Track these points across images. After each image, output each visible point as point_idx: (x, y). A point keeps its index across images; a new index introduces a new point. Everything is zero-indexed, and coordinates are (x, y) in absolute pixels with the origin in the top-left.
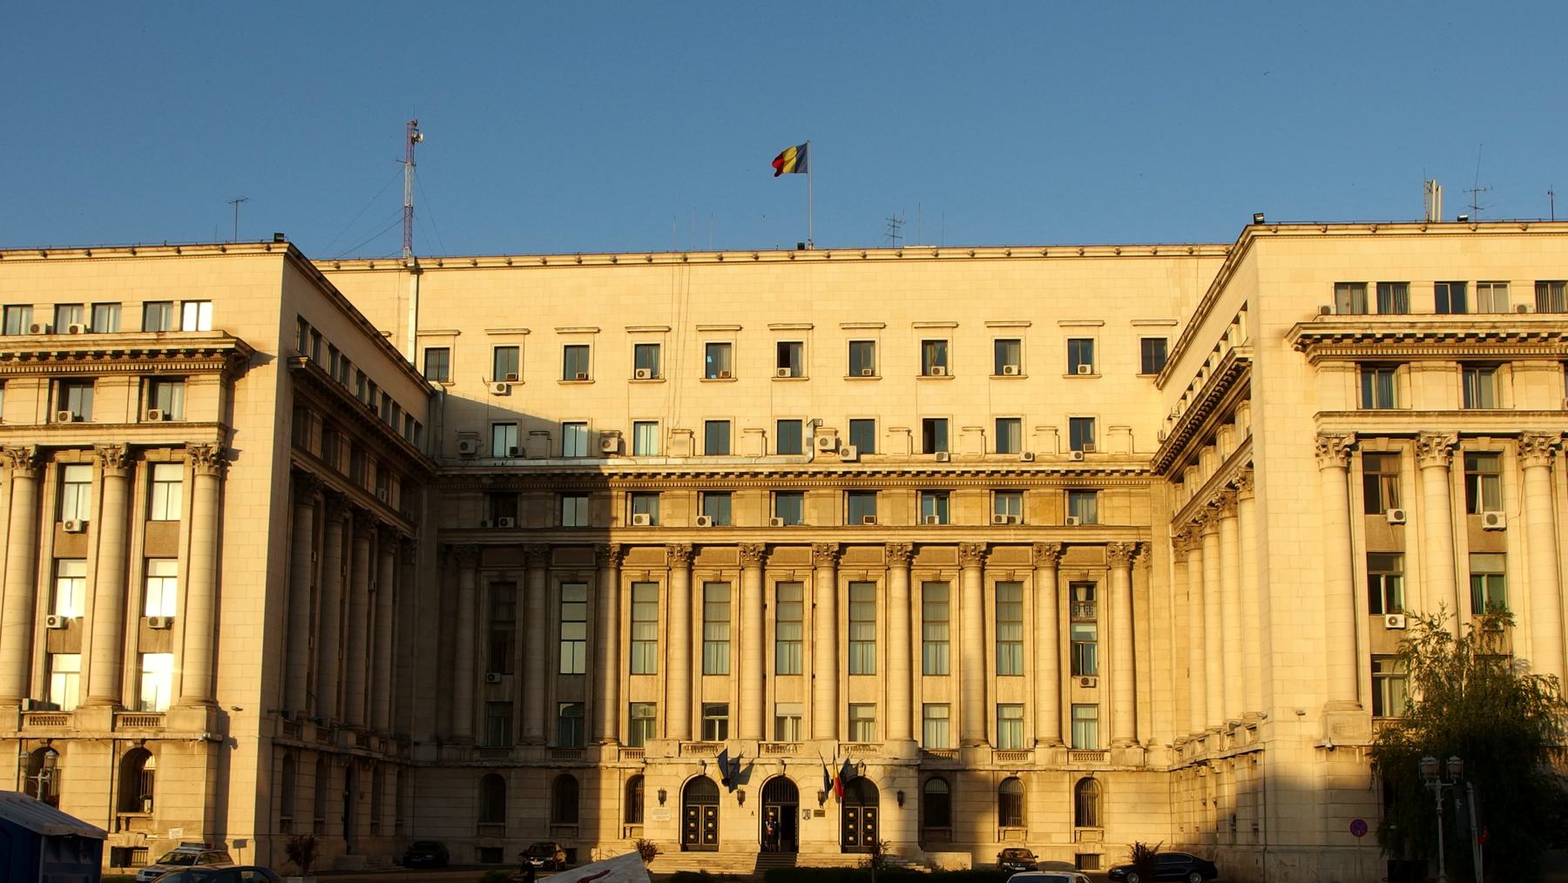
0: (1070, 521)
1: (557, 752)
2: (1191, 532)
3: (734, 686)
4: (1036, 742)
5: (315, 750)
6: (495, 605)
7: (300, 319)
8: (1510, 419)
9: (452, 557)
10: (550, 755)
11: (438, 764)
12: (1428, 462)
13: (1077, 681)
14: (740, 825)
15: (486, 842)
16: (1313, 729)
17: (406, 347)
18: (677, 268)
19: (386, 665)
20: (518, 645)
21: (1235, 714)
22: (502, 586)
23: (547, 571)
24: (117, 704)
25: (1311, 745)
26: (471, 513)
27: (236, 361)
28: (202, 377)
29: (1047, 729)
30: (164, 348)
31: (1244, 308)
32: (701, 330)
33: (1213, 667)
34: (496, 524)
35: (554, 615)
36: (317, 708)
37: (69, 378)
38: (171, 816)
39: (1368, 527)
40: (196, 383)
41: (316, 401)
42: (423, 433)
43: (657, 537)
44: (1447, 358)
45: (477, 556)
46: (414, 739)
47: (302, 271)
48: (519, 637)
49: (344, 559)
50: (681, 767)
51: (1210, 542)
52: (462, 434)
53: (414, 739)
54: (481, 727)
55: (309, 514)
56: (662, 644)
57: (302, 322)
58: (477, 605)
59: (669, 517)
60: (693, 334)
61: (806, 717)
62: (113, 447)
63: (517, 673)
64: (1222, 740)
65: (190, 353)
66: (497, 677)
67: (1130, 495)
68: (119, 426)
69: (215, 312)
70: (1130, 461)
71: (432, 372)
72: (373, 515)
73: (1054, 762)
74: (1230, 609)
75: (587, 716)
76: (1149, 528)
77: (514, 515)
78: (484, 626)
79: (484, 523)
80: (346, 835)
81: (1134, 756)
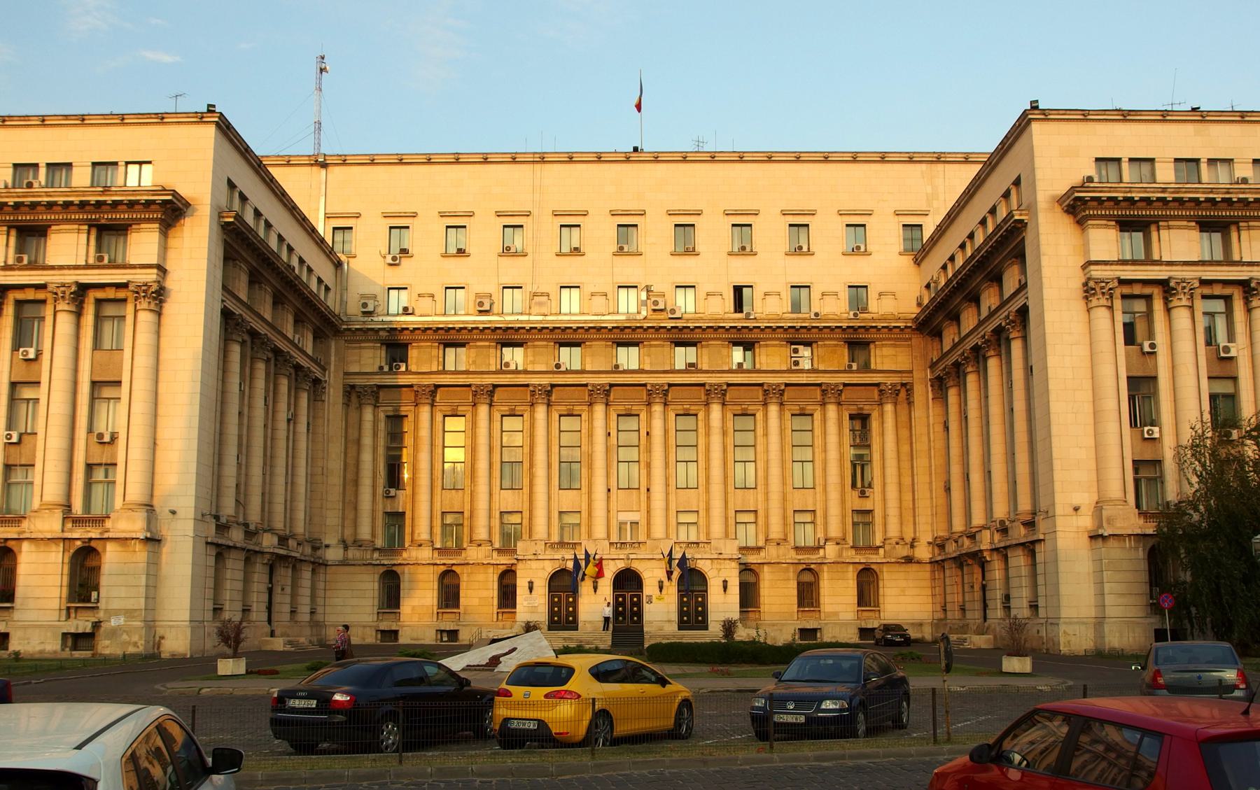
0: (850, 366)
1: (442, 551)
2: (947, 378)
3: (585, 498)
4: (826, 540)
5: (243, 549)
7: (229, 181)
8: (1239, 268)
9: (351, 392)
10: (436, 554)
11: (344, 563)
12: (1175, 303)
13: (856, 494)
14: (595, 604)
15: (384, 626)
16: (1086, 521)
18: (538, 166)
19: (301, 480)
22: (396, 420)
24: (68, 507)
25: (1086, 536)
26: (370, 359)
27: (170, 211)
28: (143, 226)
30: (109, 199)
31: (1017, 183)
32: (556, 215)
34: (391, 369)
35: (438, 442)
37: (30, 231)
38: (115, 605)
39: (1127, 355)
40: (138, 230)
42: (331, 295)
43: (522, 379)
44: (1188, 218)
47: (231, 141)
49: (267, 391)
50: (547, 562)
51: (972, 380)
52: (363, 296)
54: (380, 531)
55: (236, 350)
56: (526, 465)
57: (231, 185)
58: (375, 435)
60: (550, 218)
61: (643, 523)
62: (63, 285)
64: (992, 536)
65: (132, 204)
67: (895, 346)
68: (69, 267)
69: (154, 172)
72: (291, 357)
73: (840, 555)
75: (466, 523)
76: (911, 372)
78: (381, 451)
79: (381, 368)
80: (269, 621)
81: (904, 551)
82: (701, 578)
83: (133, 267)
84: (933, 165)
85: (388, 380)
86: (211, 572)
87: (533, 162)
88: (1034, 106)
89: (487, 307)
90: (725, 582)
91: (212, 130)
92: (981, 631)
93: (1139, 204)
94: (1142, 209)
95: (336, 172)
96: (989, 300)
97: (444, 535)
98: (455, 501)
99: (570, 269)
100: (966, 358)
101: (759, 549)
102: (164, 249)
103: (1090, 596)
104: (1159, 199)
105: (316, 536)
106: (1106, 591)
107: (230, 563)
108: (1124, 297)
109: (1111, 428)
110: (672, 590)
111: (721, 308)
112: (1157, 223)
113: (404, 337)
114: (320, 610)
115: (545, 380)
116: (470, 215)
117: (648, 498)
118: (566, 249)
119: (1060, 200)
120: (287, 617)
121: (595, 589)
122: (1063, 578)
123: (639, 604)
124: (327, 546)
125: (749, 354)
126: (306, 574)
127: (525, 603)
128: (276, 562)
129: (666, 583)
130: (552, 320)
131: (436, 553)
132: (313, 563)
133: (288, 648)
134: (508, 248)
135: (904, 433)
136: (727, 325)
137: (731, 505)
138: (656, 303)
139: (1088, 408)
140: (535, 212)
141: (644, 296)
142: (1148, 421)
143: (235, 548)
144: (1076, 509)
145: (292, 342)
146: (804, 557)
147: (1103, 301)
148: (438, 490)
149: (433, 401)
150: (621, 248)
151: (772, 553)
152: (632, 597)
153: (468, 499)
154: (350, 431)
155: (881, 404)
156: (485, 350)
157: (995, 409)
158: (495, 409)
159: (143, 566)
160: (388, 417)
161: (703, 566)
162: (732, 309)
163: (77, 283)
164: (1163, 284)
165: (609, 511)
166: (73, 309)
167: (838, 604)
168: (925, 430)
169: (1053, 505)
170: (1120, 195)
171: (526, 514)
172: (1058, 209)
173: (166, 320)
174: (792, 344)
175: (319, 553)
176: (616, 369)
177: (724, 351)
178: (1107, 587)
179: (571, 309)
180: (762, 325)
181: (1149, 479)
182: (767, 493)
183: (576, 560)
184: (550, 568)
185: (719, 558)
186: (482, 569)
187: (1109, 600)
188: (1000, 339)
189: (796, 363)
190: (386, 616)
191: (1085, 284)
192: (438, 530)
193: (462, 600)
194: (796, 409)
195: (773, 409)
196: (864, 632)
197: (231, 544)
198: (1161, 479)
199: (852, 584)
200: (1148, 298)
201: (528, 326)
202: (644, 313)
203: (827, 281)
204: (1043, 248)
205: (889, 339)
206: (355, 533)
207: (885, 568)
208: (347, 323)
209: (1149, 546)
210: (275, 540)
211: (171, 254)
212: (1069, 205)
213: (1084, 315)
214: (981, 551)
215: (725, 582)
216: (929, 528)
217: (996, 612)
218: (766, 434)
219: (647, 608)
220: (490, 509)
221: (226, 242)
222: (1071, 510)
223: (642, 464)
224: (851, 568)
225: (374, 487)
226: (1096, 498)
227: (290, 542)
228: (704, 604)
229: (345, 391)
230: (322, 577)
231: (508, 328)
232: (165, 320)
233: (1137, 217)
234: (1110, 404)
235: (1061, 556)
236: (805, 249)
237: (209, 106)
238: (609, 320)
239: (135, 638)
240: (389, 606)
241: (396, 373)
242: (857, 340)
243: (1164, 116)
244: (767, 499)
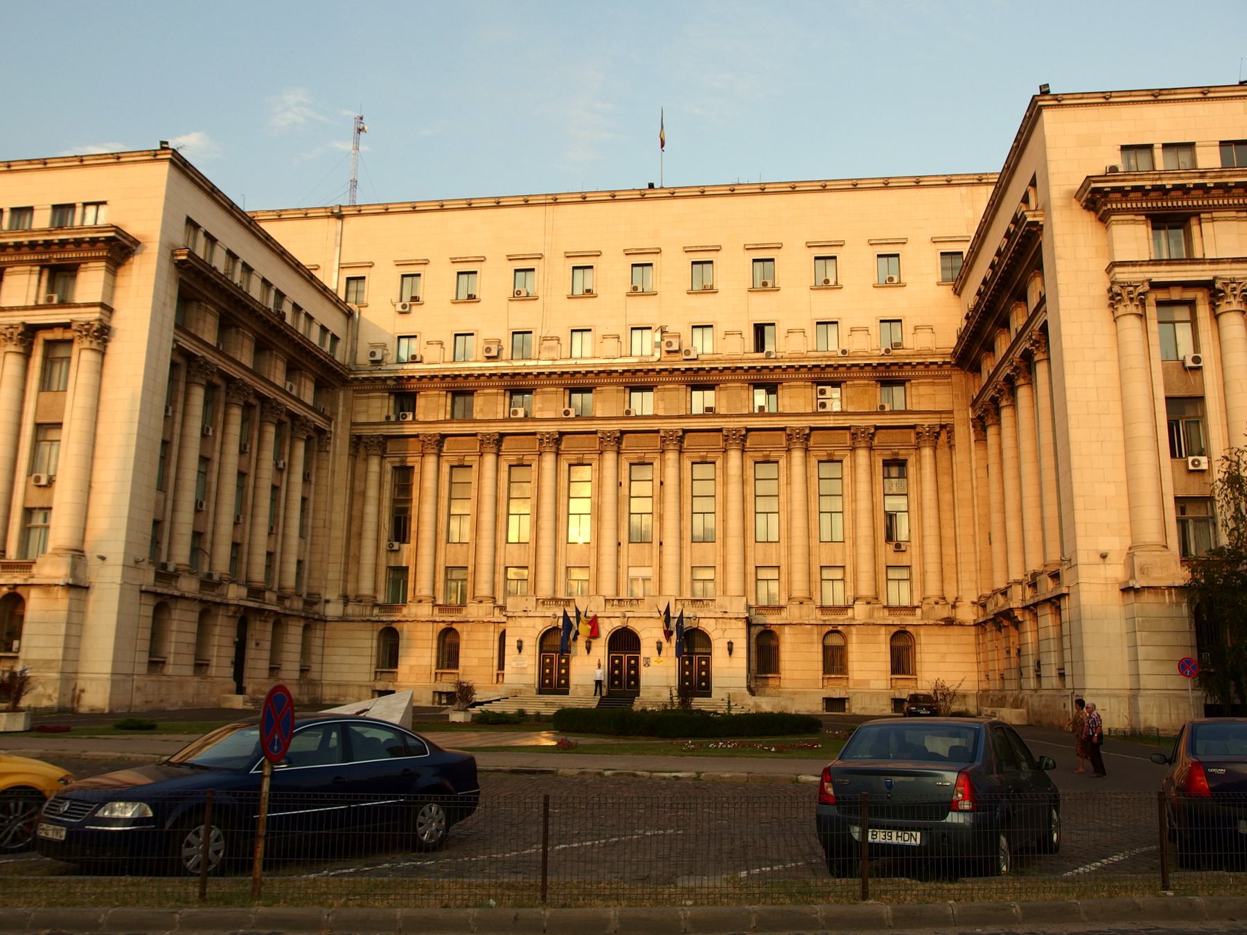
1: (444, 608)
2: (986, 415)
7: (189, 221)
9: (359, 445)
11: (343, 619)
12: (1224, 307)
14: (588, 667)
16: (1116, 571)
17: (331, 277)
20: (414, 519)
21: (1034, 564)
25: (1117, 589)
26: (377, 409)
27: (118, 249)
28: (91, 264)
31: (1033, 183)
33: (1012, 525)
34: (398, 418)
36: (211, 564)
40: (86, 270)
41: (208, 295)
42: (340, 345)
43: (529, 427)
45: (382, 444)
47: (192, 180)
48: (414, 512)
51: (1006, 414)
52: (372, 345)
58: (381, 485)
59: (541, 410)
60: (562, 260)
62: (11, 326)
64: (1024, 590)
66: (396, 545)
67: (934, 384)
70: (933, 355)
71: (352, 297)
73: (871, 616)
74: (1028, 468)
76: (951, 412)
78: (386, 503)
79: (388, 418)
81: (945, 612)
82: (706, 639)
83: (78, 306)
84: (974, 189)
85: (395, 430)
86: (148, 622)
87: (545, 204)
88: (1044, 91)
89: (494, 353)
90: (730, 644)
91: (165, 167)
92: (1017, 704)
93: (1173, 193)
94: (1177, 199)
95: (351, 223)
96: (1018, 320)
97: (447, 590)
98: (457, 556)
99: (582, 312)
100: (1000, 391)
101: (780, 608)
102: (111, 287)
103: (1124, 667)
104: (1197, 186)
105: (315, 591)
106: (1140, 657)
107: (177, 614)
108: (1159, 304)
109: (1145, 458)
110: (670, 649)
111: (740, 349)
112: (1198, 215)
113: (412, 386)
114: (315, 667)
115: (553, 428)
116: (482, 260)
117: (661, 552)
118: (578, 291)
119: (1078, 196)
121: (589, 649)
122: (1088, 641)
123: (636, 667)
124: (327, 601)
125: (773, 397)
126: (294, 633)
127: (514, 664)
128: (244, 619)
129: (665, 644)
130: (564, 364)
131: (436, 610)
132: (306, 618)
133: (250, 706)
134: (519, 293)
135: (945, 480)
136: (746, 365)
137: (750, 561)
138: (669, 344)
139: (1118, 435)
140: (546, 255)
141: (658, 337)
142: (1196, 450)
144: (1104, 556)
145: (283, 391)
146: (831, 618)
147: (1132, 308)
148: (442, 543)
150: (635, 288)
151: (793, 613)
152: (629, 659)
154: (357, 483)
155: (918, 448)
156: (492, 398)
157: (1027, 446)
158: (502, 459)
159: (63, 614)
160: (395, 468)
161: (707, 626)
162: (752, 349)
163: (23, 323)
164: (1208, 285)
165: (618, 566)
166: (21, 350)
167: (869, 671)
168: (967, 477)
169: (1075, 551)
170: (1148, 184)
172: (1076, 206)
173: (109, 359)
174: (819, 384)
175: (316, 608)
176: (628, 416)
177: (744, 394)
178: (1141, 650)
179: (585, 354)
180: (784, 365)
181: (1197, 520)
182: (789, 548)
183: (566, 617)
184: (540, 626)
185: (724, 617)
186: (482, 627)
187: (1144, 667)
188: (1028, 362)
189: (823, 405)
190: (384, 675)
191: (1110, 290)
192: (440, 586)
193: (461, 661)
194: (823, 455)
195: (797, 455)
196: (897, 703)
197: (176, 593)
198: (1211, 520)
200: (1191, 304)
201: (535, 371)
202: (657, 355)
203: (855, 317)
204: (1058, 251)
205: (926, 377)
206: (357, 589)
207: (922, 631)
210: (243, 592)
211: (119, 293)
212: (1087, 200)
213: (1108, 327)
214: (1011, 610)
215: (730, 644)
216: (973, 586)
217: (419, 658)
218: (789, 483)
219: (644, 671)
220: (494, 564)
222: (1097, 558)
224: (883, 630)
225: (378, 540)
226: (1128, 543)
227: (267, 595)
228: (707, 668)
230: (319, 633)
231: (515, 374)
232: (108, 359)
233: (1172, 211)
234: (1142, 429)
235: (1086, 613)
236: (832, 282)
237: (162, 143)
238: (620, 363)
239: (50, 691)
241: (402, 423)
243: (1205, 94)
244: (789, 554)
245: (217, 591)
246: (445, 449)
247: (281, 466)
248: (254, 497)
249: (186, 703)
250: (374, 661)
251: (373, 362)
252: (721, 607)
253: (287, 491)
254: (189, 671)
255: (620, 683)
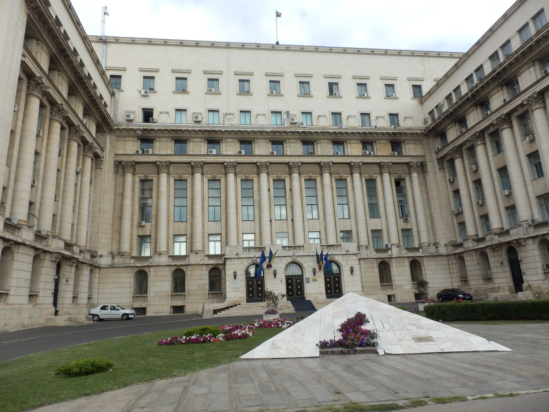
3: (257, 225)
6: (143, 191)
9: (120, 166)
11: (112, 266)
14: (276, 285)
15: (138, 305)
23: (168, 174)
29: (394, 239)
32: (236, 74)
43: (220, 159)
46: (100, 253)
50: (245, 260)
52: (127, 112)
53: (100, 253)
58: (133, 190)
63: (153, 222)
66: (143, 223)
67: (415, 144)
73: (400, 253)
76: (424, 156)
77: (152, 148)
78: (137, 199)
79: (137, 152)
80: (55, 304)
81: (432, 250)
90: (352, 268)
114: (95, 296)
115: (233, 160)
117: (293, 225)
120: (70, 300)
126: (86, 272)
128: (61, 261)
138: (293, 119)
143: (24, 244)
149: (169, 171)
153: (189, 227)
171: (224, 235)
175: (95, 260)
186: (199, 268)
190: (138, 299)
193: (186, 287)
197: (19, 240)
199: (408, 268)
203: (379, 111)
207: (424, 259)
208: (117, 125)
209: (209, 269)
210: (62, 244)
215: (352, 268)
221: (29, 16)
223: (288, 206)
225: (132, 221)
229: (115, 165)
230: (97, 275)
240: (140, 292)
242: (396, 141)
245: (44, 243)
246: (171, 170)
247: (79, 170)
248: (64, 186)
249: (23, 325)
250: (132, 290)
251: (128, 121)
252: (345, 248)
253: (81, 187)
254: (25, 300)
255: (253, 295)
